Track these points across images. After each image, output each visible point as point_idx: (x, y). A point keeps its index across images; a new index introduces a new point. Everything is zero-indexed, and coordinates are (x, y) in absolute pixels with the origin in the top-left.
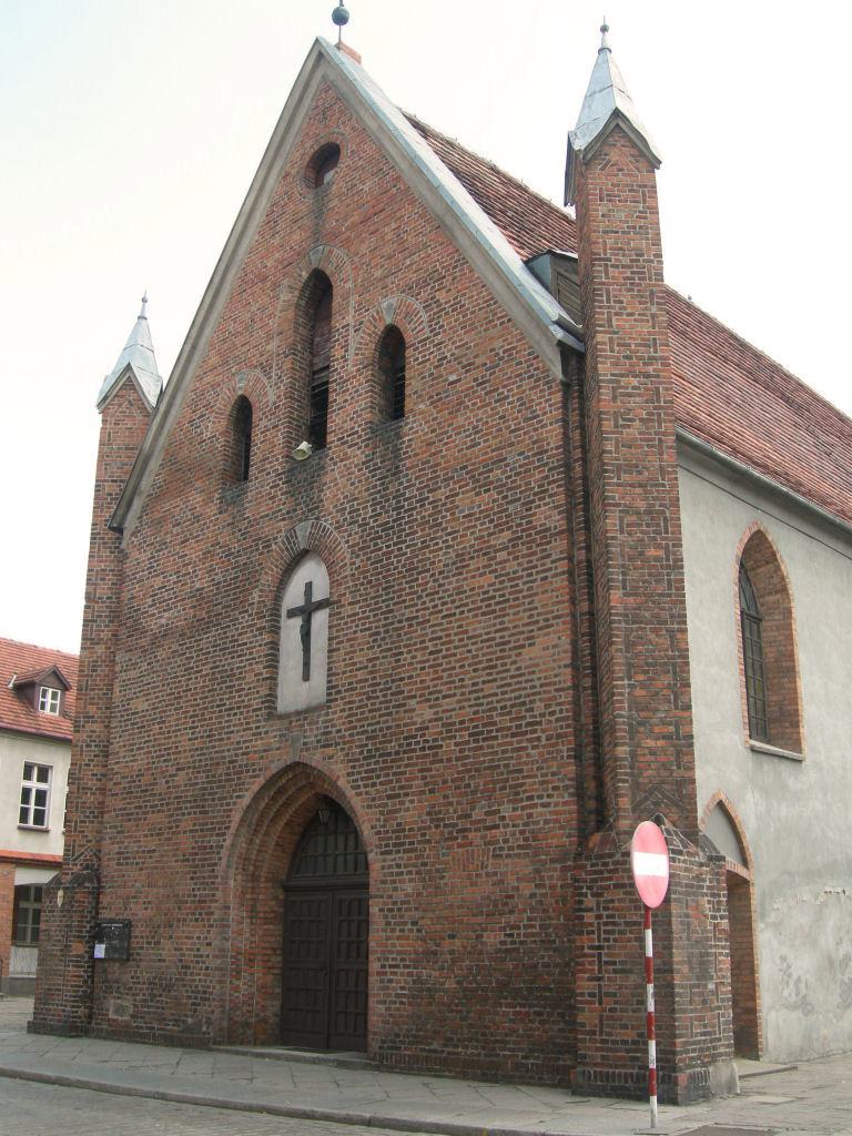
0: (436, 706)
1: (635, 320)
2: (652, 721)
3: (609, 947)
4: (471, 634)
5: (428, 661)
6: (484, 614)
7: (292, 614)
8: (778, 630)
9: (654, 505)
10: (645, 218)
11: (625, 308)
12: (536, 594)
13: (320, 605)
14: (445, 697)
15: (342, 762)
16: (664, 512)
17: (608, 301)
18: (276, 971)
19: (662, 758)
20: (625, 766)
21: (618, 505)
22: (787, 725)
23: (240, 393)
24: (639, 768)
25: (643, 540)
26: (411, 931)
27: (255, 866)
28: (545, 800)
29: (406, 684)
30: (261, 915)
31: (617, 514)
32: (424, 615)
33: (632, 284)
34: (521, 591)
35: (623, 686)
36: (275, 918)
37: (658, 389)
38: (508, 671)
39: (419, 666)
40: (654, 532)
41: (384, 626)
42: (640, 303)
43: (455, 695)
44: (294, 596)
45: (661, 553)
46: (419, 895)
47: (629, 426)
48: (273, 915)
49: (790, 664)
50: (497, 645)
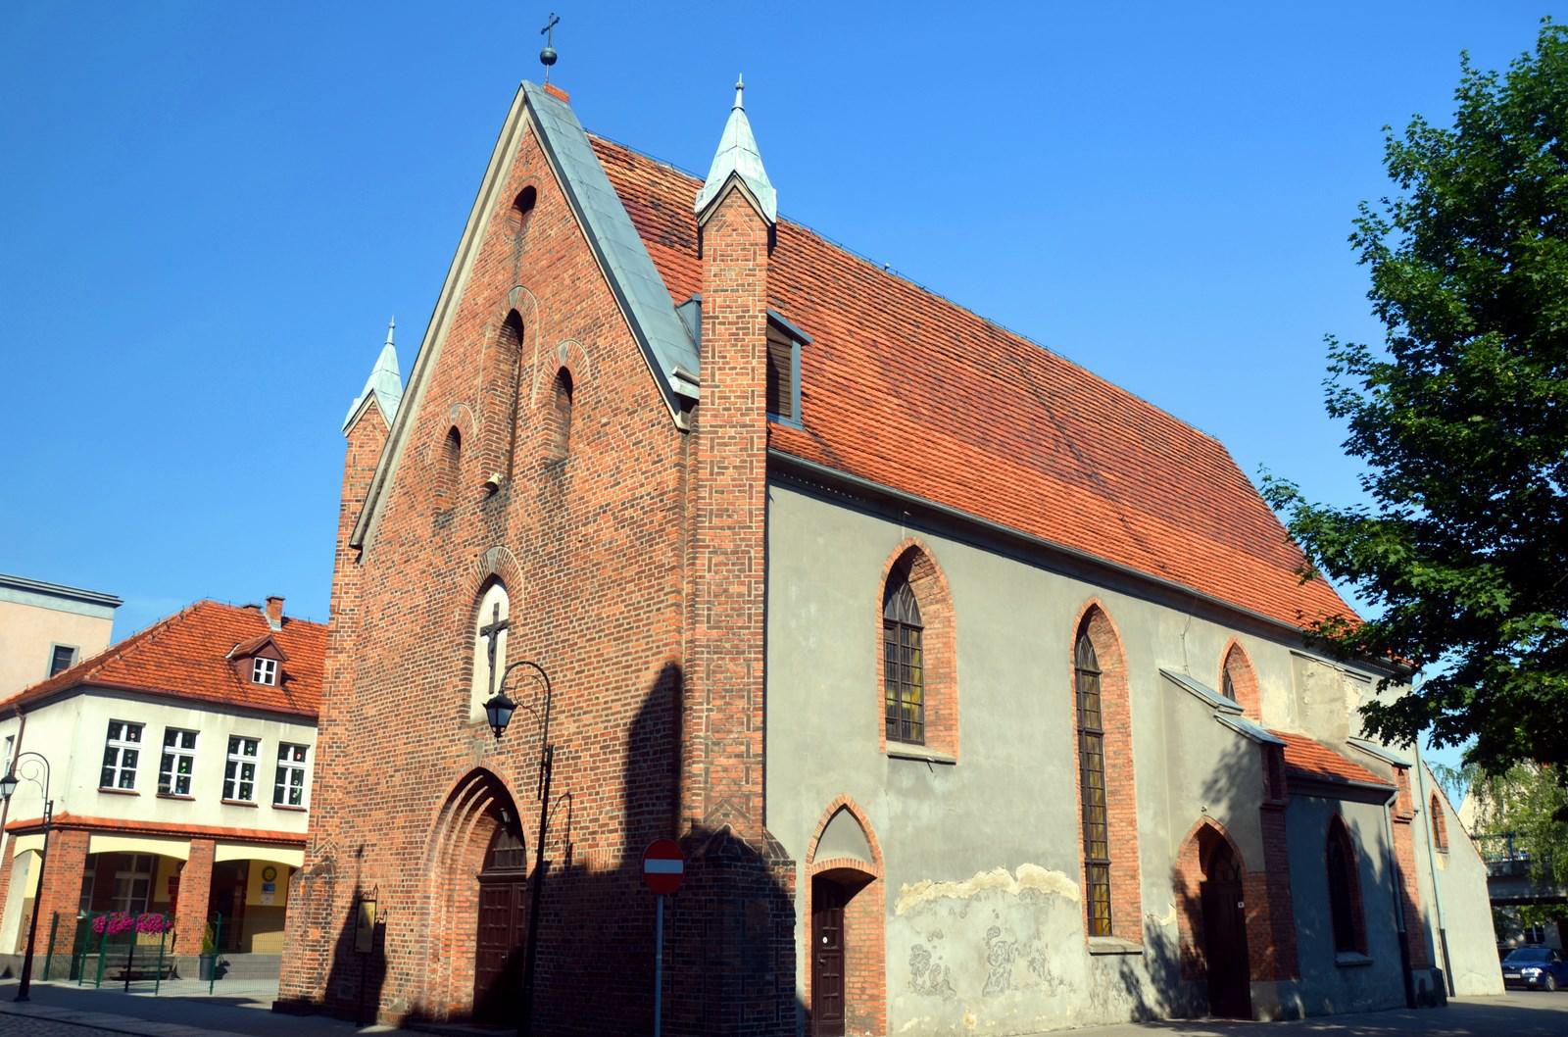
0: (578, 720)
1: (737, 374)
2: (726, 742)
3: (680, 941)
4: (605, 657)
5: (574, 680)
6: (615, 640)
7: (484, 632)
8: (938, 638)
9: (740, 546)
10: (754, 275)
11: (728, 363)
12: (652, 623)
13: (504, 625)
14: (585, 713)
15: (511, 768)
16: (749, 552)
17: (713, 357)
18: (470, 955)
19: (733, 775)
20: (699, 782)
21: (708, 547)
22: (942, 728)
23: (453, 424)
24: (712, 784)
25: (728, 578)
26: (554, 921)
27: (452, 860)
28: (651, 808)
29: (559, 700)
30: (457, 904)
31: (707, 555)
32: (573, 639)
33: (736, 340)
34: (642, 620)
35: (702, 711)
36: (470, 907)
37: (752, 438)
38: (630, 691)
39: (568, 684)
40: (739, 570)
41: (546, 646)
42: (742, 357)
43: (591, 711)
44: (485, 618)
45: (744, 590)
46: (561, 889)
47: (723, 474)
48: (468, 904)
49: (135, 859)
50: (623, 668)
